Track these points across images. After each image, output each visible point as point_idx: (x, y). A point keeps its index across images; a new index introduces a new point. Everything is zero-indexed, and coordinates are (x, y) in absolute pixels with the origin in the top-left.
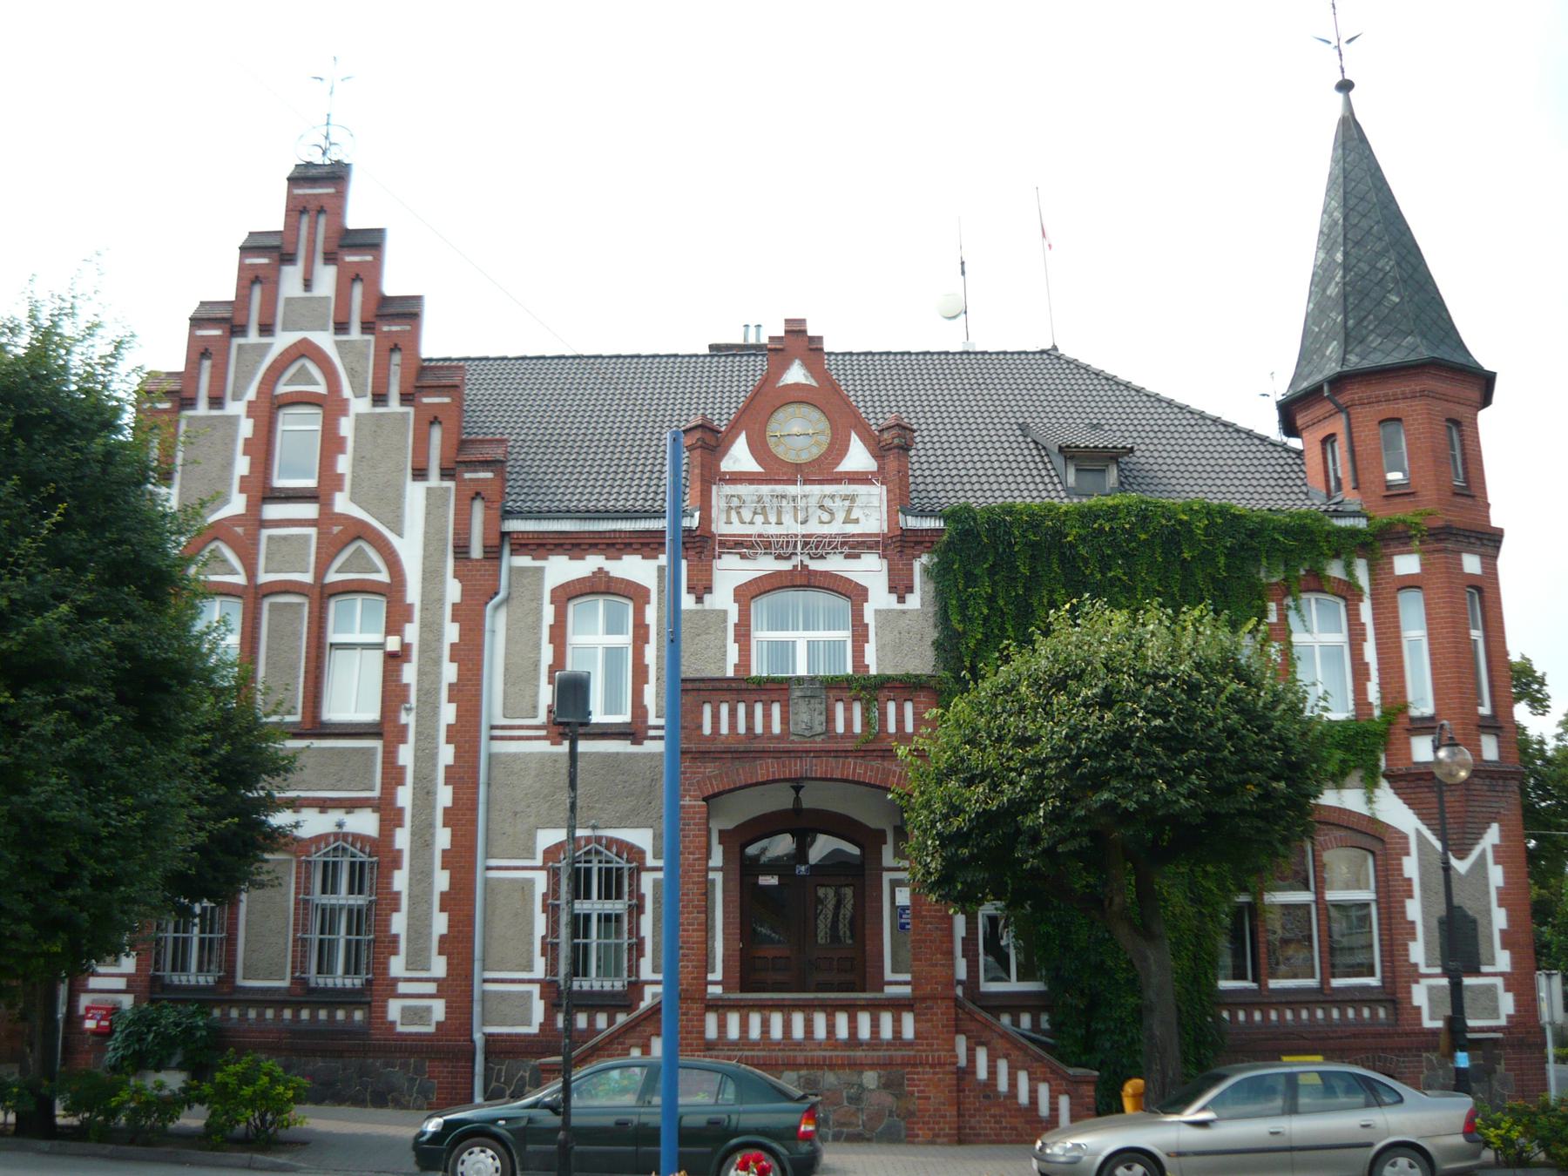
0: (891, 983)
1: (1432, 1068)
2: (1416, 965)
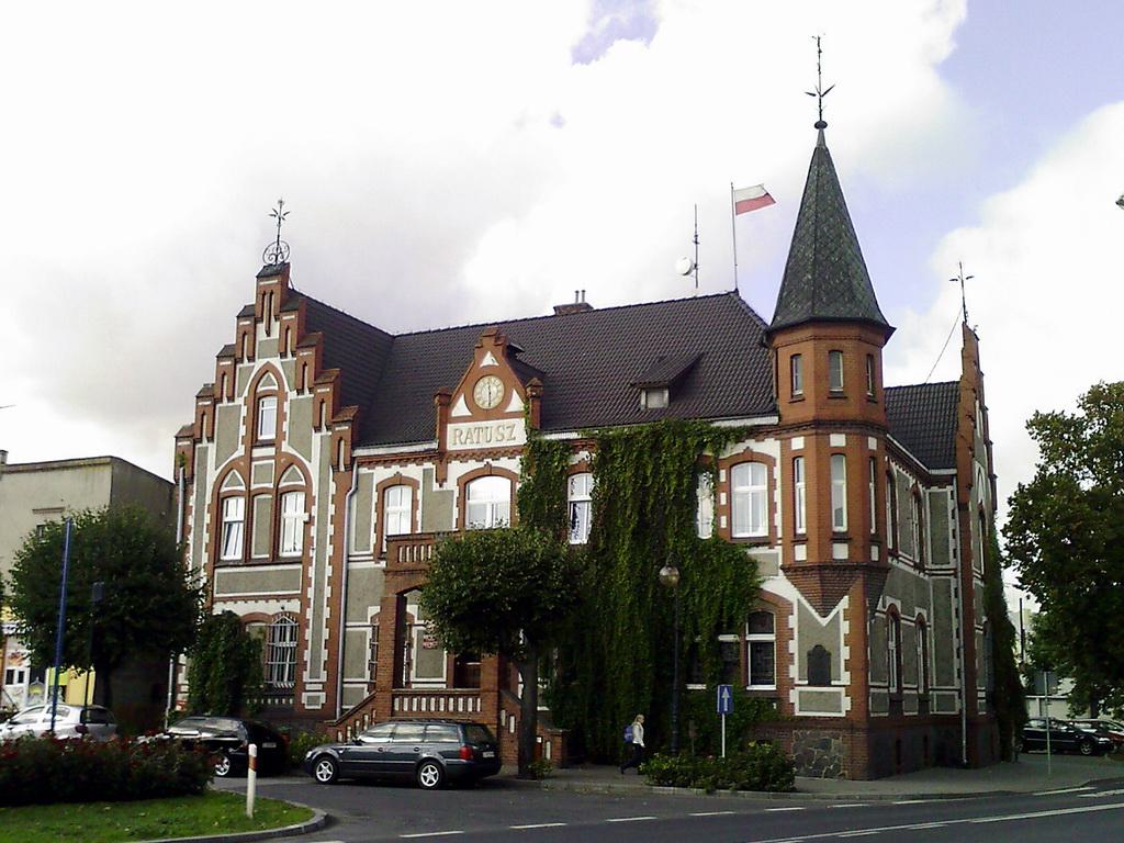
2: (793, 679)
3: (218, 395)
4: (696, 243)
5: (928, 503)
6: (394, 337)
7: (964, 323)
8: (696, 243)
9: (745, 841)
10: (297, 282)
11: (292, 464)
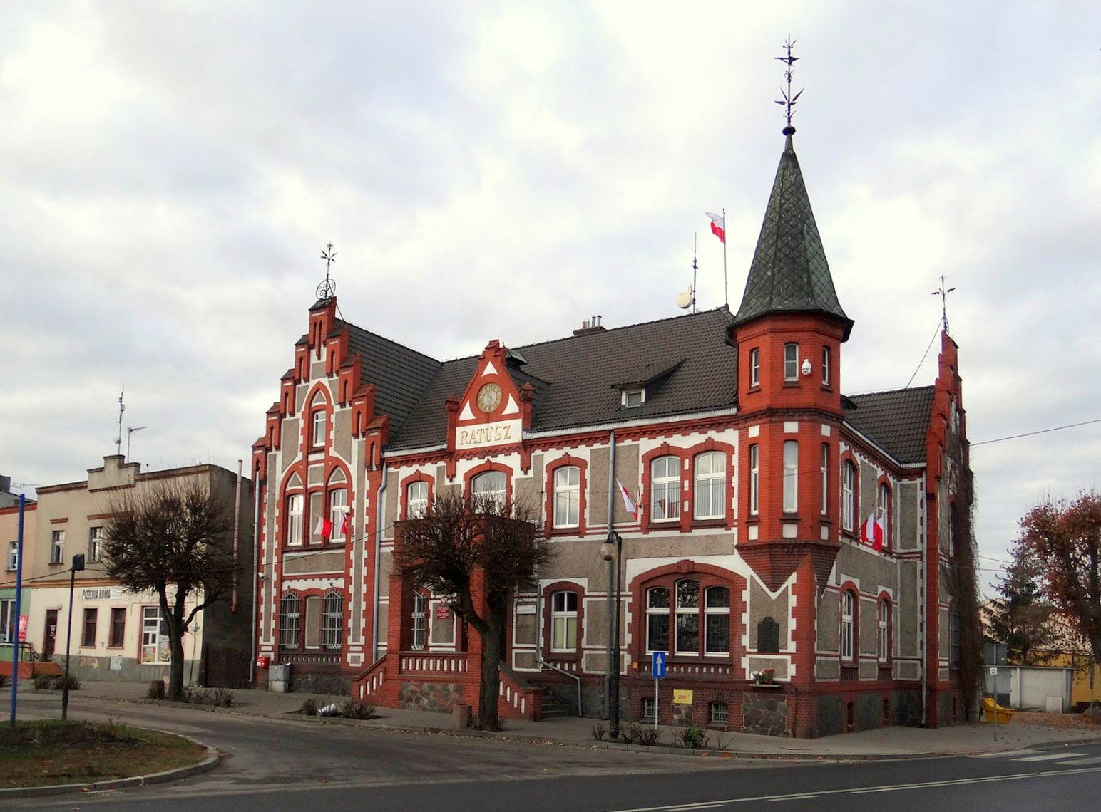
1: (748, 700)
3: (282, 412)
4: (695, 267)
5: (899, 495)
6: (443, 364)
7: (944, 333)
8: (695, 267)
9: (607, 810)
10: (344, 312)
11: (337, 467)
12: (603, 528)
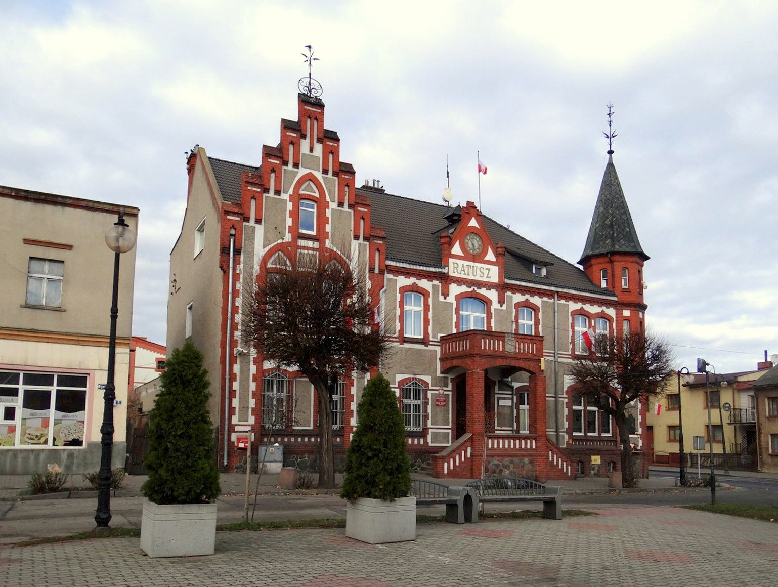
0: (497, 430)
12: (551, 353)
